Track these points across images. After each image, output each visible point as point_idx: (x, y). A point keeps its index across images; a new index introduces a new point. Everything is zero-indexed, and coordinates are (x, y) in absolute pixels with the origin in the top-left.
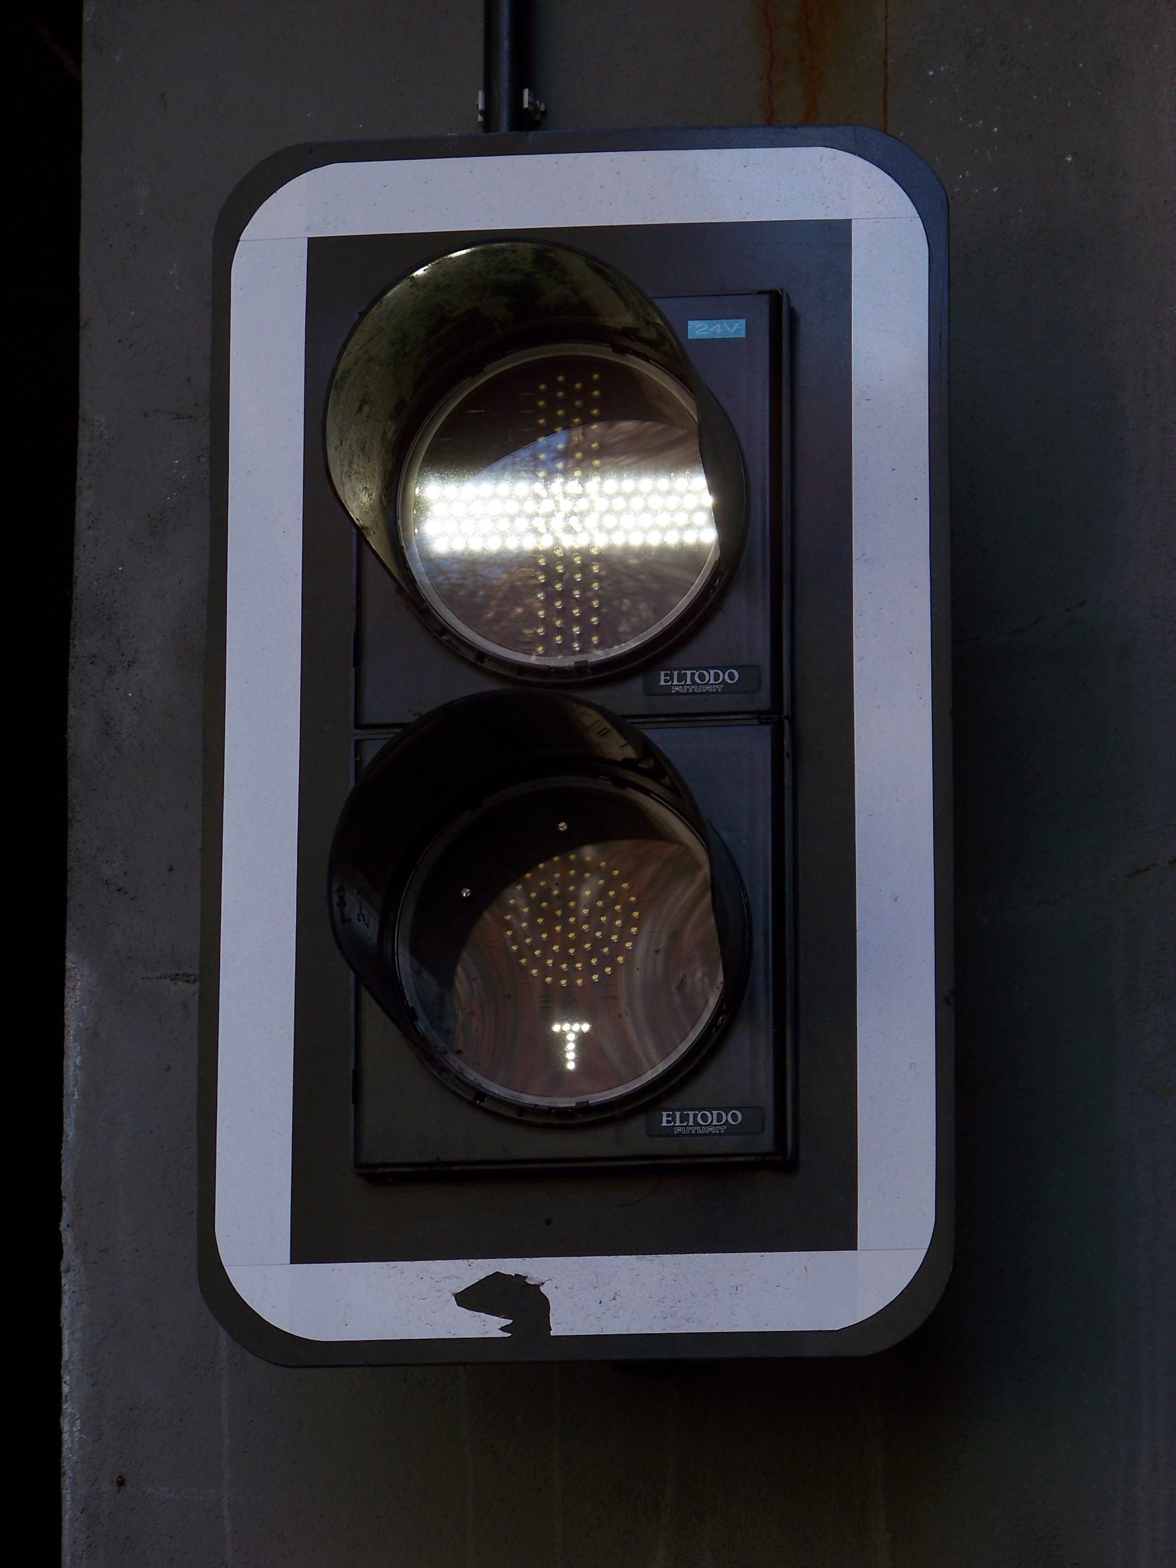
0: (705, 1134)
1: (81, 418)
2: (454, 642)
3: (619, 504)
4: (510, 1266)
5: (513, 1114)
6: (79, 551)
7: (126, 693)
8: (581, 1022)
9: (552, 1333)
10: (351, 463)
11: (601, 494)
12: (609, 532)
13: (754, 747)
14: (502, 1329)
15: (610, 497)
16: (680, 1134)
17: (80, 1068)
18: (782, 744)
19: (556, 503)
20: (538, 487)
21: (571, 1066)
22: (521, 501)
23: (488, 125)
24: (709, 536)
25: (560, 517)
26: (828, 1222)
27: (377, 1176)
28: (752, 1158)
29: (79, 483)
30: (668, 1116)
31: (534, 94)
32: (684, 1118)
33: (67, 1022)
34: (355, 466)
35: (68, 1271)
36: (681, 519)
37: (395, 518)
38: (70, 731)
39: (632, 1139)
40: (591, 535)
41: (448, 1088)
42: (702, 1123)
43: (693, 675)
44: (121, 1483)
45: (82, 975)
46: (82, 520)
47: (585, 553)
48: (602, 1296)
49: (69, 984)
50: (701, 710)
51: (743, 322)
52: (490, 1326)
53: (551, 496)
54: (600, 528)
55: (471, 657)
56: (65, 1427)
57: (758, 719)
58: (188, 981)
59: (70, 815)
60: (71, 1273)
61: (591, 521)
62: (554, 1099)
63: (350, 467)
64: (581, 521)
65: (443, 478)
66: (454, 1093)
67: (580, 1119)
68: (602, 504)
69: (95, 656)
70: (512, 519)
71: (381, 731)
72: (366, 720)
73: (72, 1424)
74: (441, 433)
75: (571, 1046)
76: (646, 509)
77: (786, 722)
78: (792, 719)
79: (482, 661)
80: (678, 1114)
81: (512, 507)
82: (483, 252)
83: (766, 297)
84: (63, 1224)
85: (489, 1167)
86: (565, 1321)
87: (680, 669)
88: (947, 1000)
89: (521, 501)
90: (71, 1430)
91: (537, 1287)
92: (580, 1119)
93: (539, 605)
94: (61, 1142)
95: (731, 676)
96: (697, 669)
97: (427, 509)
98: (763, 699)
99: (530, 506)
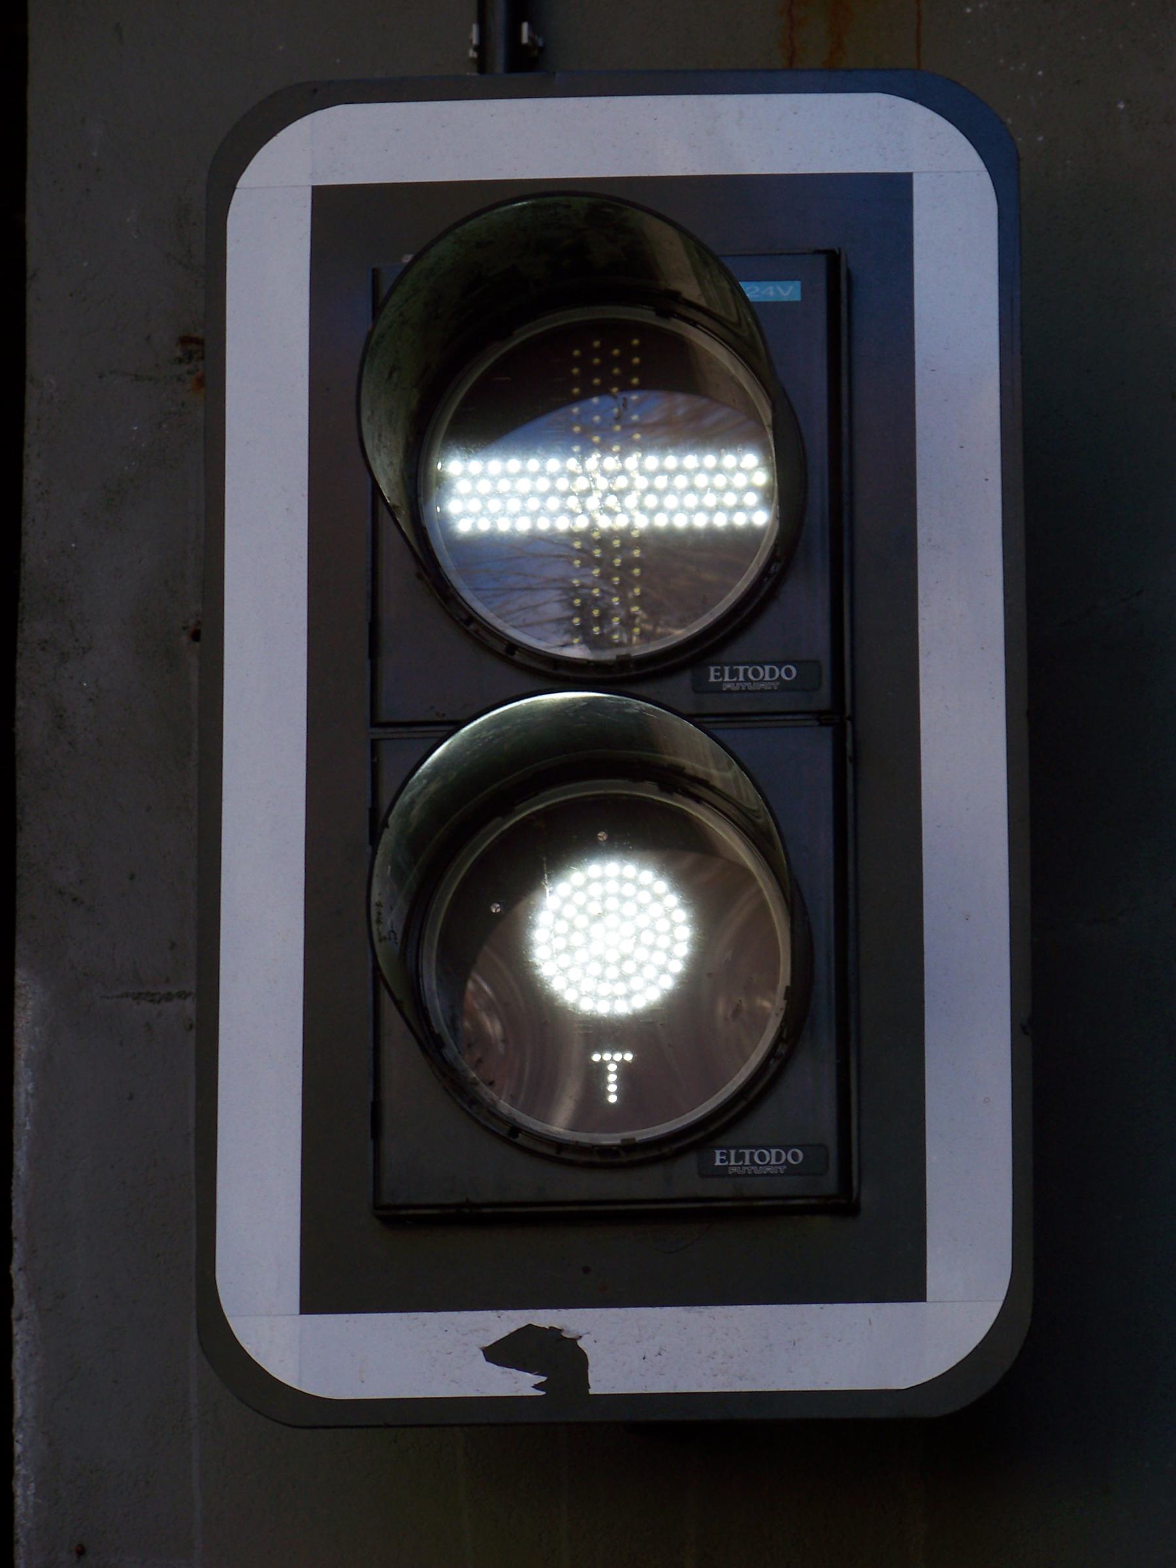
0: (763, 1175)
1: (28, 379)
2: (482, 632)
3: (661, 482)
4: (544, 1318)
5: (551, 1151)
6: (26, 525)
7: (81, 683)
8: (623, 1051)
9: (591, 1392)
10: (380, 435)
11: (642, 472)
12: (652, 513)
13: (815, 749)
14: (536, 1387)
15: (652, 475)
16: (735, 1175)
17: (32, 1096)
18: (845, 748)
19: (631, 480)
20: (572, 463)
21: (613, 1099)
22: (553, 478)
23: (482, 65)
24: (762, 518)
25: (597, 495)
26: (897, 1274)
27: (395, 1218)
28: (813, 1201)
29: (27, 451)
30: (722, 1154)
31: (532, 29)
32: (739, 1157)
33: (17, 1045)
34: (383, 439)
35: (19, 1319)
36: (730, 499)
37: (417, 496)
38: (18, 724)
39: (685, 1180)
40: (590, 516)
41: (477, 1122)
42: (761, 1161)
43: (746, 671)
44: (81, 1552)
45: (34, 993)
46: (30, 490)
47: (624, 535)
48: (642, 1350)
49: (19, 1003)
50: (755, 709)
51: (798, 284)
52: (522, 1384)
53: (586, 474)
54: (641, 508)
55: (501, 648)
56: (18, 1491)
57: (818, 719)
58: (152, 1001)
59: (19, 817)
60: (24, 1322)
61: (631, 501)
62: (596, 1135)
63: (380, 440)
64: (620, 501)
65: (469, 453)
66: (485, 1128)
67: (624, 1158)
68: (642, 483)
69: (46, 642)
70: (524, 498)
71: (400, 729)
72: (384, 717)
73: (26, 1488)
74: (465, 403)
75: (612, 1078)
76: (692, 488)
77: (849, 724)
78: (852, 718)
79: (513, 654)
80: (733, 1152)
81: (543, 484)
82: (533, 206)
83: (822, 260)
84: (14, 1267)
85: (584, 1208)
86: (604, 1379)
87: (731, 664)
88: (1024, 1028)
89: (553, 478)
90: (24, 1494)
91: (574, 1341)
92: (624, 1158)
93: (613, 591)
94: (11, 1176)
95: (788, 673)
96: (751, 664)
97: (452, 486)
98: (823, 698)
99: (563, 484)
